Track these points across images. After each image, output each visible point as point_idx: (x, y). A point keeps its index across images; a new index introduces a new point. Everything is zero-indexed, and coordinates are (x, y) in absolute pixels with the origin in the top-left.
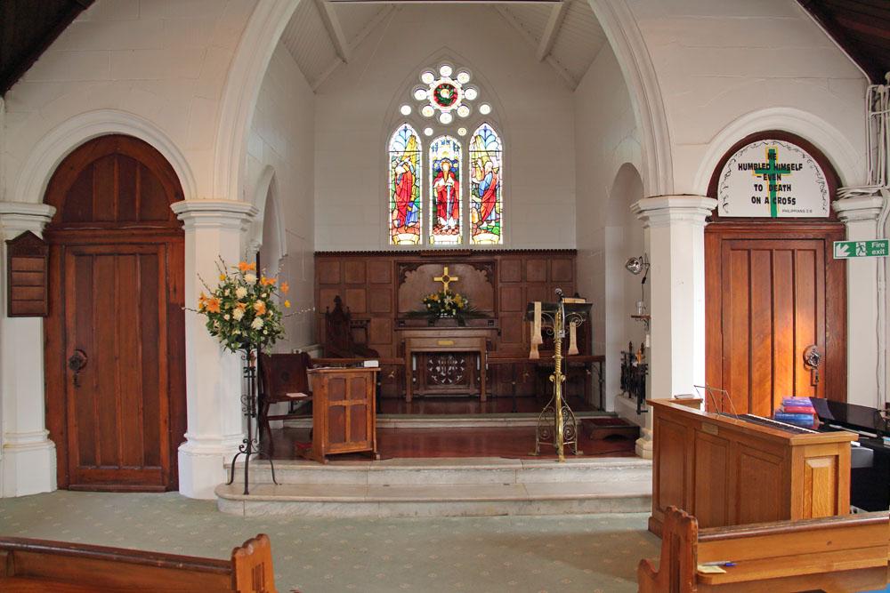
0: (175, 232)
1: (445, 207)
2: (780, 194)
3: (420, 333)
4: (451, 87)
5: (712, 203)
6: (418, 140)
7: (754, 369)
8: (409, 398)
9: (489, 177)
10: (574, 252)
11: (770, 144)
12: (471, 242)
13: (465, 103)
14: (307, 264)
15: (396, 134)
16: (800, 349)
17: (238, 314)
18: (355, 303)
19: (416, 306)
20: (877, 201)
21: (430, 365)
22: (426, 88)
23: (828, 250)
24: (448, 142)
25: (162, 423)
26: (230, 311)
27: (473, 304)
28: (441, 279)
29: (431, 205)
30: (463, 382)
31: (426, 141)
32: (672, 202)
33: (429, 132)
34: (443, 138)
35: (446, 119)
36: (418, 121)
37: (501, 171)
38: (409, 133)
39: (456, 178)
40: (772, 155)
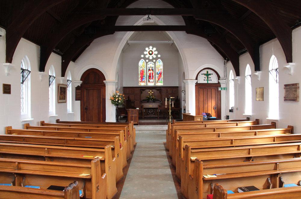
0: (104, 86)
1: (151, 77)
2: (209, 79)
3: (145, 104)
4: (152, 51)
5: (196, 81)
6: (145, 62)
7: (204, 110)
8: (143, 118)
9: (160, 71)
10: (178, 87)
11: (207, 70)
12: (156, 85)
13: (155, 54)
14: (122, 89)
15: (140, 61)
16: (213, 106)
17: (117, 100)
18: (132, 98)
19: (145, 98)
20: (225, 81)
21: (147, 111)
22: (147, 51)
23: (218, 89)
24: (151, 63)
25: (101, 119)
26: (115, 99)
27: (157, 98)
28: (150, 93)
29: (148, 77)
30: (154, 115)
31: (147, 63)
32: (188, 81)
33: (147, 61)
34: (150, 62)
35: (151, 58)
36: (145, 59)
37: (162, 70)
38: (143, 61)
39: (153, 71)
40: (207, 72)
